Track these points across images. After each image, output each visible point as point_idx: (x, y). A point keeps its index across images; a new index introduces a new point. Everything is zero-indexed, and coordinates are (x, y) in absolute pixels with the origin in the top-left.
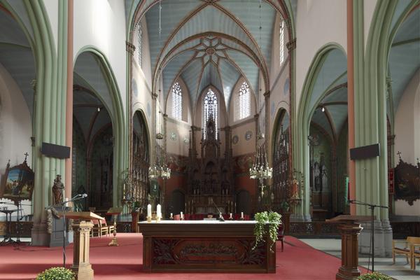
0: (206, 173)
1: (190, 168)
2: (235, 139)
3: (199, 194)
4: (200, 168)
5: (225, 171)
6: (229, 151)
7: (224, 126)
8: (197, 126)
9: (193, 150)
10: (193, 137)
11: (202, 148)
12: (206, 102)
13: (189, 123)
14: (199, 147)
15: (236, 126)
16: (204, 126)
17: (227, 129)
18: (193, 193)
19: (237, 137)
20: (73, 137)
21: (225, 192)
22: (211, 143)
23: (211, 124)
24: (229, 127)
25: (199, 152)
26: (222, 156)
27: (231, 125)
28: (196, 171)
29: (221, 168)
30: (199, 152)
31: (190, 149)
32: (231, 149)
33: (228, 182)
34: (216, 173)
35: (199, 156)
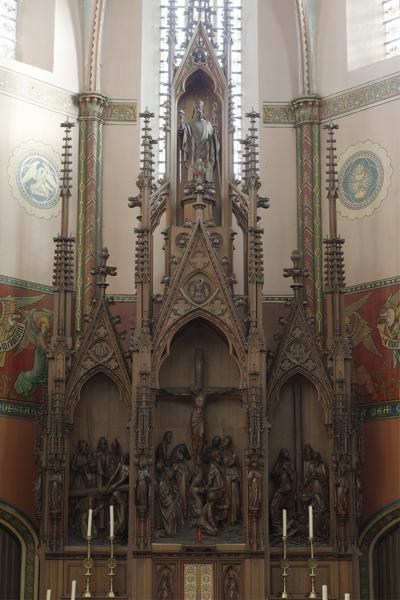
0: (164, 396)
1: (58, 367)
2: (359, 175)
3: (122, 535)
4: (127, 358)
5: (298, 382)
6: (319, 256)
7: (286, 97)
8: (115, 94)
9: (79, 252)
10: (86, 164)
11: (144, 233)
12: (264, 339)
13: (65, 77)
14: (121, 230)
15: (362, 97)
16: (154, 89)
17: (308, 116)
18: (77, 534)
19: (369, 165)
20: (259, 7)
21: (298, 521)
22: (201, 198)
23: (199, 85)
24: (317, 103)
25: (124, 258)
26: (276, 284)
27: (329, 88)
28: (100, 378)
29: (272, 358)
30: (124, 258)
31: (63, 241)
32: (336, 242)
33: (318, 460)
34: (232, 395)
35: (123, 284)
